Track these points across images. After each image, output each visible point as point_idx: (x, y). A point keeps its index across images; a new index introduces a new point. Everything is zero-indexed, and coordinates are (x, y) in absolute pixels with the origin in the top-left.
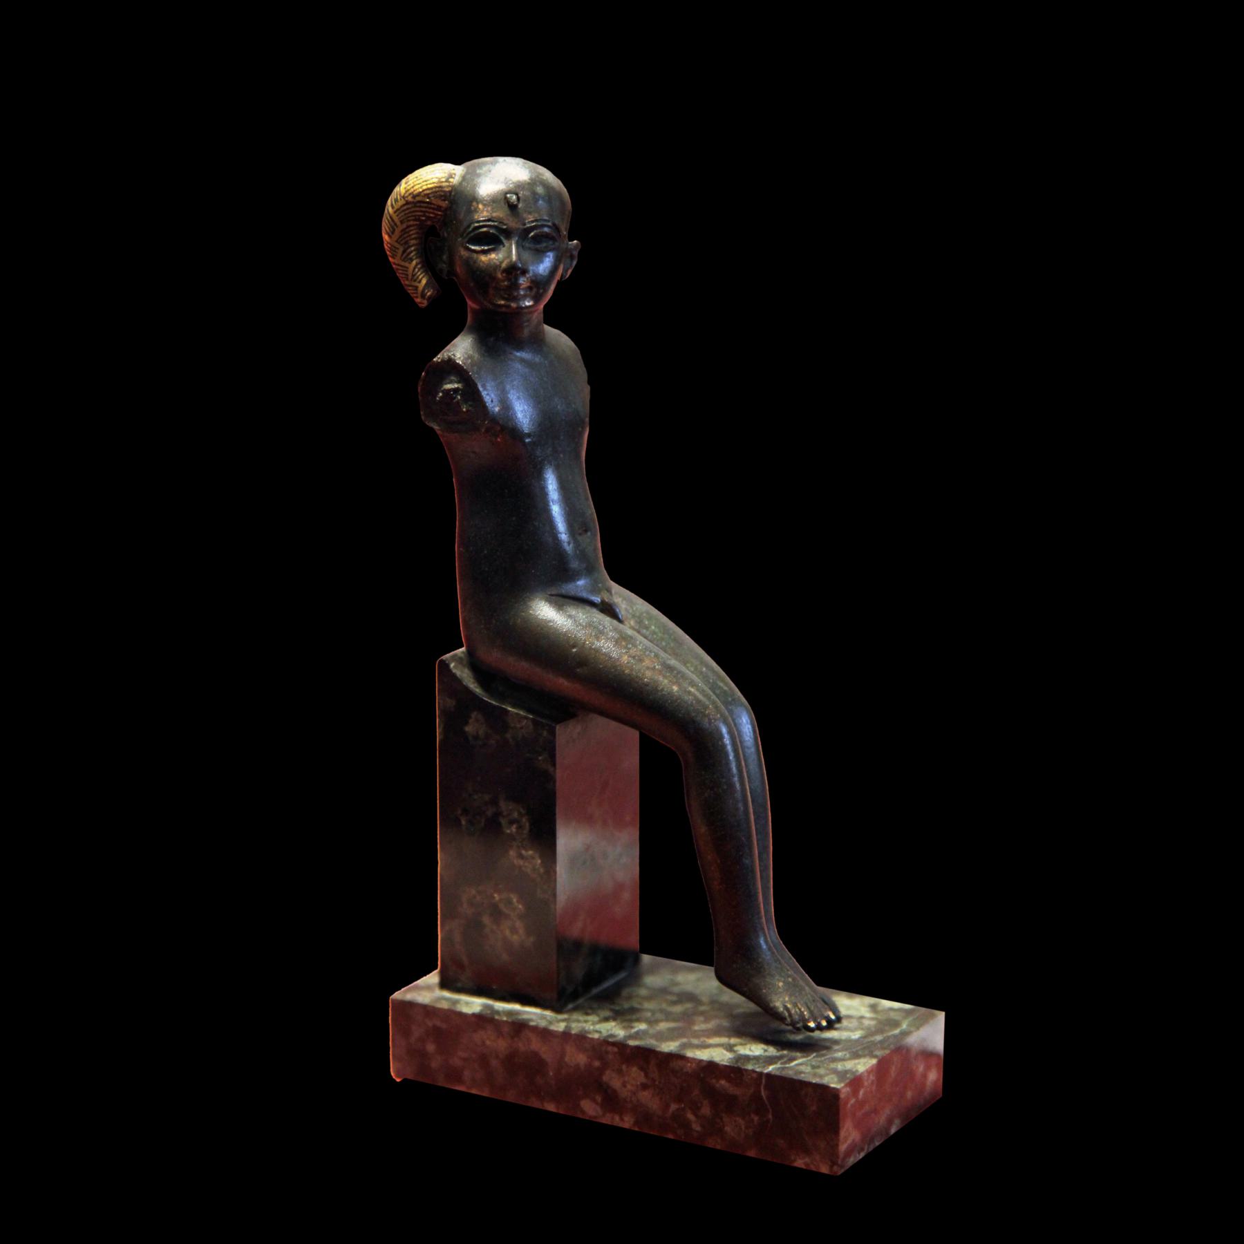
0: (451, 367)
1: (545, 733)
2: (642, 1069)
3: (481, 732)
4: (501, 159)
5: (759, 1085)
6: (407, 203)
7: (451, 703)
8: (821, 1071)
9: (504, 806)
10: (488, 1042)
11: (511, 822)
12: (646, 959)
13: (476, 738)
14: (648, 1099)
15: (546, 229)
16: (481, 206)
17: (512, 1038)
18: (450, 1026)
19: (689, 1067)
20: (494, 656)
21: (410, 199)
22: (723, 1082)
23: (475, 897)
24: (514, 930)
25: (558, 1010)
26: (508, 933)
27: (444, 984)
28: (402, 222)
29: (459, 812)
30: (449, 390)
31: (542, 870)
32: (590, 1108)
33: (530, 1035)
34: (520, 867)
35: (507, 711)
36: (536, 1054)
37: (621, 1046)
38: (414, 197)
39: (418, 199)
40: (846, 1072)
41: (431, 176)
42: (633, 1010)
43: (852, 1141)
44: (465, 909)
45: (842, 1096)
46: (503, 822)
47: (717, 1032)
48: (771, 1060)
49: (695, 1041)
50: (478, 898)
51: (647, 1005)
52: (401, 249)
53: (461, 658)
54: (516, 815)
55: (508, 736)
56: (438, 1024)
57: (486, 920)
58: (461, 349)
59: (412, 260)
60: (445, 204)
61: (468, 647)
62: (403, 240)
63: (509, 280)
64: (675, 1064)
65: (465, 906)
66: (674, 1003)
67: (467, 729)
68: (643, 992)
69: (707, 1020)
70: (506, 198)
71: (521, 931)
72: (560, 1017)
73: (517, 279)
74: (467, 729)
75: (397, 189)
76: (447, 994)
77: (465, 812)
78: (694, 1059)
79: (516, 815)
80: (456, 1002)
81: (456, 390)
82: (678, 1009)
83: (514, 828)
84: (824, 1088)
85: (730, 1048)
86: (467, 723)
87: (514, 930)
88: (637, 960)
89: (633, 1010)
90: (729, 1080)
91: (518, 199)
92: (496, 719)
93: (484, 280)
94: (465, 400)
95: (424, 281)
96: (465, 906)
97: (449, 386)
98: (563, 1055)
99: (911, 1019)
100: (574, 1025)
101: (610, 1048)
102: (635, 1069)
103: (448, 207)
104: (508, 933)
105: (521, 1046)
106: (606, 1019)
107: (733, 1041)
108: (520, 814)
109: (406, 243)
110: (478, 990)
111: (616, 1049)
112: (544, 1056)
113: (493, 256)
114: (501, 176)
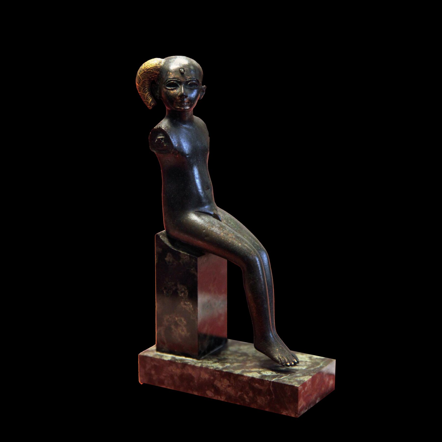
0: (160, 131)
1: (194, 260)
2: (228, 380)
3: (171, 260)
4: (178, 57)
5: (270, 386)
6: (145, 72)
7: (160, 250)
8: (292, 381)
9: (179, 286)
10: (173, 370)
11: (182, 292)
12: (230, 341)
13: (169, 262)
14: (230, 391)
15: (194, 82)
16: (171, 73)
17: (182, 369)
18: (160, 365)
19: (245, 379)
20: (175, 233)
21: (146, 71)
22: (257, 384)
23: (169, 319)
24: (183, 331)
25: (198, 359)
26: (180, 331)
27: (158, 350)
28: (143, 79)
29: (163, 288)
30: (160, 139)
31: (192, 309)
32: (210, 394)
33: (188, 368)
34: (185, 308)
35: (180, 253)
36: (190, 375)
37: (221, 372)
38: (147, 70)
39: (148, 71)
40: (301, 381)
41: (153, 63)
42: (225, 359)
43: (303, 406)
44: (165, 323)
45: (299, 389)
46: (179, 292)
47: (255, 367)
48: (274, 377)
49: (247, 370)
50: (170, 319)
51: (230, 357)
52: (143, 89)
53: (164, 234)
54: (183, 290)
55: (181, 261)
56: (156, 364)
57: (173, 327)
58: (164, 124)
59: (146, 92)
60: (158, 73)
61: (166, 230)
62: (143, 85)
63: (181, 99)
64: (240, 378)
65: (165, 322)
66: (240, 356)
67: (166, 259)
68: (228, 352)
69: (251, 363)
70: (180, 70)
71: (185, 331)
72: (199, 361)
73: (184, 99)
74: (166, 259)
75: (141, 67)
76: (159, 353)
77: (165, 288)
78: (247, 376)
79: (183, 290)
80: (162, 356)
81: (162, 139)
82: (241, 358)
83: (183, 294)
84: (293, 387)
85: (259, 372)
86: (166, 257)
87: (183, 331)
88: (226, 341)
89: (225, 359)
90: (259, 384)
91: (184, 71)
92: (176, 255)
93: (172, 99)
94: (165, 142)
95: (151, 100)
96: (165, 322)
97: (159, 137)
98: (200, 375)
99: (324, 362)
100: (204, 364)
101: (217, 372)
102: (225, 380)
103: (159, 73)
104: (180, 331)
105: (185, 372)
106: (215, 362)
107: (260, 370)
108: (185, 289)
109: (144, 86)
110: (170, 352)
111: (219, 373)
112: (193, 375)
113: (175, 91)
114: (178, 62)
